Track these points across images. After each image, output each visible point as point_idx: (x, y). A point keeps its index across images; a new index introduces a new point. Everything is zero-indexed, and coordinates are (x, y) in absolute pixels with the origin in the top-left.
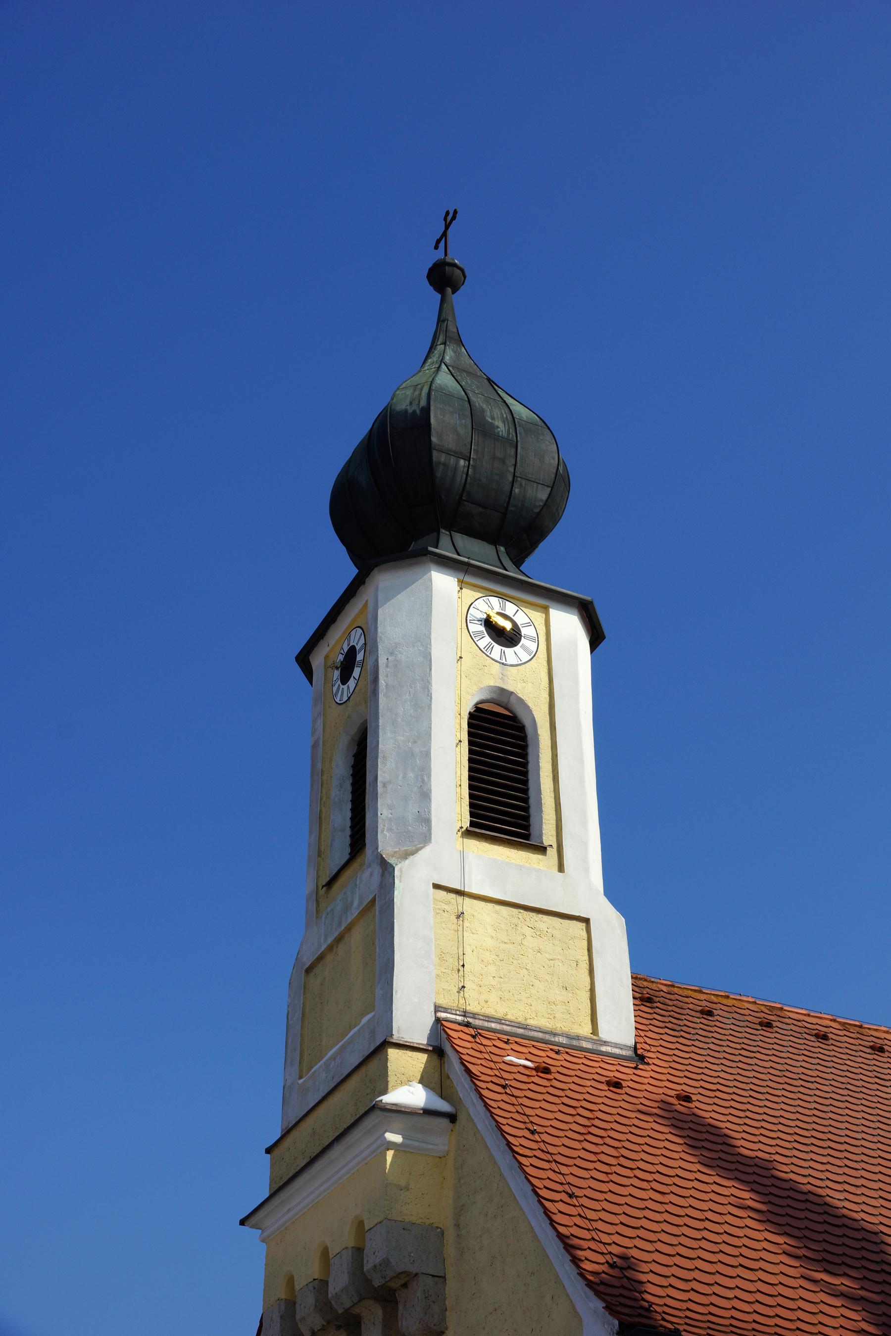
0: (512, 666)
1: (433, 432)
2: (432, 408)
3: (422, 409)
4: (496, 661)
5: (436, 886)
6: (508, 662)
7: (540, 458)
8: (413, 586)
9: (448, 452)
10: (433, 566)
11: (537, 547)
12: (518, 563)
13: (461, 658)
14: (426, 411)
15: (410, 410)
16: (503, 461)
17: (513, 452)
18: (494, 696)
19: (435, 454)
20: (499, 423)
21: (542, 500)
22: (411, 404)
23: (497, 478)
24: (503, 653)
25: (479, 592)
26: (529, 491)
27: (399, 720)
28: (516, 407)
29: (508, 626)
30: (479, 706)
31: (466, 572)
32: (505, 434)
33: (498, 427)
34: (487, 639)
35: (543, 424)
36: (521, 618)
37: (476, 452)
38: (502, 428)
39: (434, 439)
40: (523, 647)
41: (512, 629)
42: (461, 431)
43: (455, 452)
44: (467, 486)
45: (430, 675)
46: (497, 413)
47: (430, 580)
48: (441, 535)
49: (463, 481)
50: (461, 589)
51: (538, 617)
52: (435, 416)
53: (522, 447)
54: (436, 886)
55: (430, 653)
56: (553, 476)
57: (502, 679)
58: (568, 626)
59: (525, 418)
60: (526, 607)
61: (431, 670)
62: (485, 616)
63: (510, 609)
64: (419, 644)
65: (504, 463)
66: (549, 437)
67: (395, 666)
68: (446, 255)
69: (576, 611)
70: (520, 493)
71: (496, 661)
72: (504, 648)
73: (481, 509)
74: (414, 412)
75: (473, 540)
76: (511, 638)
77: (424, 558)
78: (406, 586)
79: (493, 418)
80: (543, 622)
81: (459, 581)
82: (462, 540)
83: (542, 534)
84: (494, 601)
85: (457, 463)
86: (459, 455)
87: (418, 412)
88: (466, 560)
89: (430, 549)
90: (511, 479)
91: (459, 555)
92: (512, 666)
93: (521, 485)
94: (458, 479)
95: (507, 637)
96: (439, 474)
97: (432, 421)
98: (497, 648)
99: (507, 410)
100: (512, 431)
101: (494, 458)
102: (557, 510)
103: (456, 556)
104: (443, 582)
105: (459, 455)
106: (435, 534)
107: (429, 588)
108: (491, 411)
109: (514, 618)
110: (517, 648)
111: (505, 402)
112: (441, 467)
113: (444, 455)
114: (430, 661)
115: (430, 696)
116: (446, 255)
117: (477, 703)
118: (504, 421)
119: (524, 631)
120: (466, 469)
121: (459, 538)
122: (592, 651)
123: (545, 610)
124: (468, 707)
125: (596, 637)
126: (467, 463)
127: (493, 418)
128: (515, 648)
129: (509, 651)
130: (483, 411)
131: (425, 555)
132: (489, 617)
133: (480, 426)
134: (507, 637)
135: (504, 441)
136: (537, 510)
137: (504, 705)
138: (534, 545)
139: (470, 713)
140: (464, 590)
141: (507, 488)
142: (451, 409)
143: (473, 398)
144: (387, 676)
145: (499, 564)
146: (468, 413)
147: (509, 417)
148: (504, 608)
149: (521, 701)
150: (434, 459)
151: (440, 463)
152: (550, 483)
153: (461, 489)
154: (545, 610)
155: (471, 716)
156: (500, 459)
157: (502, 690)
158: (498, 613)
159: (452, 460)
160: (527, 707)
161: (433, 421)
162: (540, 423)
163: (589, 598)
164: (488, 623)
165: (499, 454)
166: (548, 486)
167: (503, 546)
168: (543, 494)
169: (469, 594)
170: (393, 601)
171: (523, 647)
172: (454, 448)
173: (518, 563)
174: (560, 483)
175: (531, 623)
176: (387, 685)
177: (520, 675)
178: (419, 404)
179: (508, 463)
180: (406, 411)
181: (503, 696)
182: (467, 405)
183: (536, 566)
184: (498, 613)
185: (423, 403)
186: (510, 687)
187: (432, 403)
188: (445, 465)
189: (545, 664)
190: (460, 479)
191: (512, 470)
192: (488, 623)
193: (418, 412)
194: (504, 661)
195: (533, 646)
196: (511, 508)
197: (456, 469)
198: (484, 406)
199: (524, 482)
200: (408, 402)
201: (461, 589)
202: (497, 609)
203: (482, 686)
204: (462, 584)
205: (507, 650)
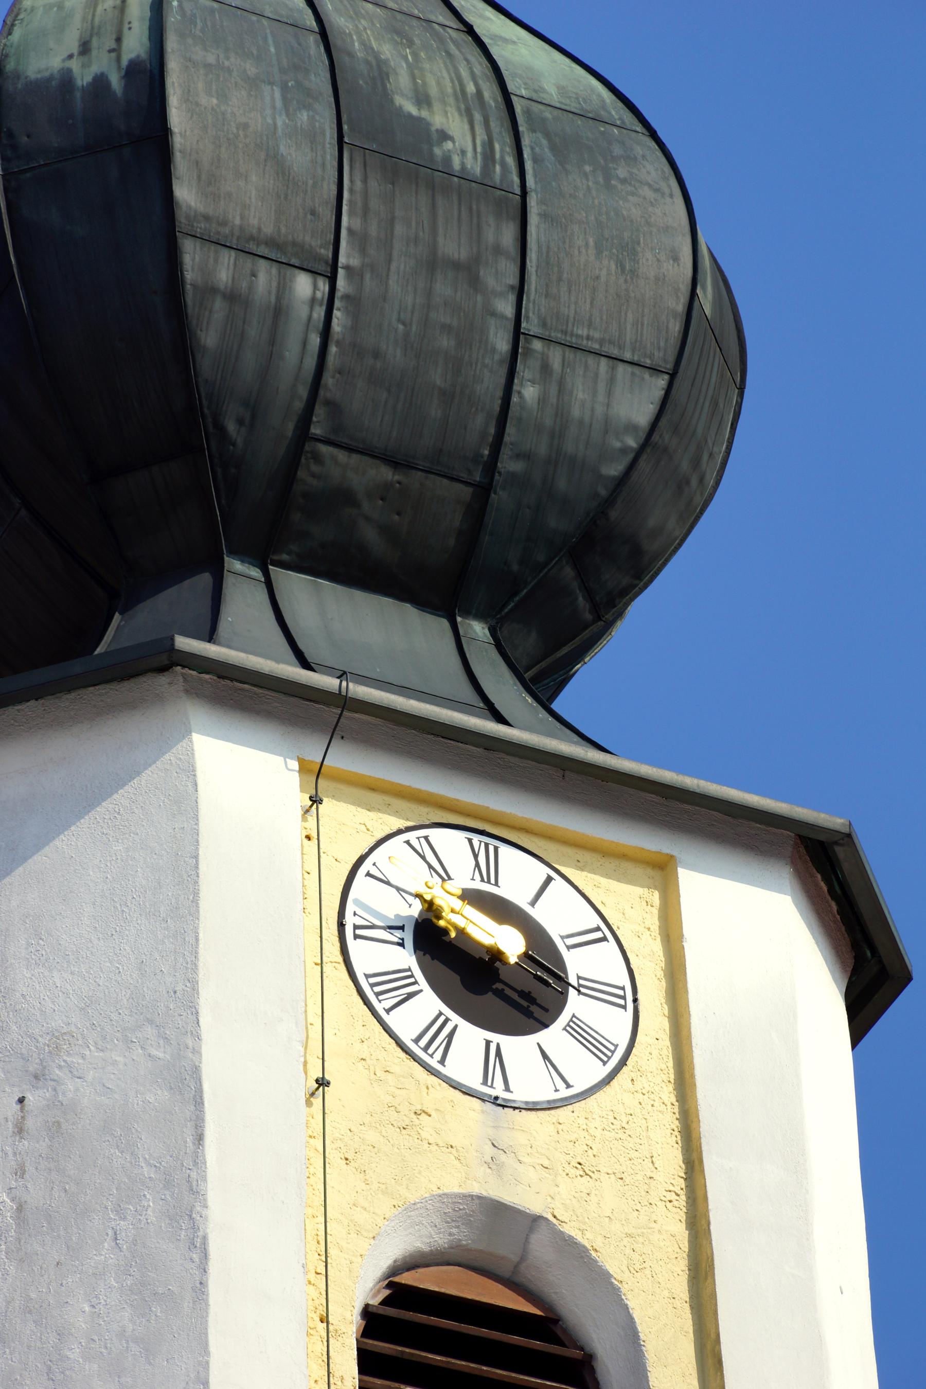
0: (533, 1107)
1: (181, 165)
2: (173, 65)
3: (132, 71)
4: (468, 1092)
5: (430, 1116)
6: (519, 1095)
7: (615, 254)
8: (121, 797)
9: (245, 247)
10: (197, 714)
11: (620, 615)
12: (544, 681)
13: (322, 1083)
14: (149, 78)
15: (83, 77)
16: (469, 272)
17: (508, 236)
18: (463, 1235)
19: (192, 257)
20: (447, 119)
21: (631, 428)
22: (85, 48)
23: (445, 342)
24: (493, 1059)
25: (387, 809)
26: (580, 393)
27: (74, 1353)
28: (518, 50)
29: (511, 944)
30: (406, 1278)
31: (334, 732)
32: (475, 167)
33: (444, 136)
34: (428, 1004)
35: (628, 118)
36: (560, 914)
37: (361, 241)
38: (461, 140)
39: (185, 193)
40: (576, 1030)
41: (526, 956)
42: (297, 157)
43: (271, 243)
44: (328, 379)
45: (198, 1161)
46: (437, 76)
47: (190, 771)
48: (229, 581)
49: (310, 363)
50: (316, 800)
51: (631, 904)
52: (188, 98)
53: (544, 216)
54: (430, 1116)
55: (196, 1072)
56: (676, 327)
57: (492, 1163)
58: (755, 939)
59: (552, 93)
60: (581, 866)
61: (200, 1139)
62: (416, 909)
63: (518, 876)
64: (150, 1031)
65: (475, 282)
66: (653, 167)
67: (55, 1129)
68: (533, 903)
69: (784, 874)
70: (542, 400)
71: (468, 1092)
72: (495, 1038)
73: (387, 474)
74: (100, 81)
75: (359, 595)
76: (527, 995)
77: (163, 680)
78: (88, 801)
79: (423, 99)
80: (654, 922)
81: (304, 768)
82: (314, 602)
83: (641, 567)
84: (453, 845)
85: (283, 288)
86: (287, 257)
87: (116, 81)
88: (330, 683)
89: (184, 643)
90: (503, 344)
91: (306, 664)
92: (533, 1107)
93: (546, 369)
94: (291, 352)
95: (500, 987)
96: (209, 337)
97: (176, 117)
98: (470, 1038)
99: (480, 66)
100: (503, 149)
101: (432, 264)
102: (696, 463)
103: (293, 671)
104: (239, 781)
105: (287, 257)
106: (205, 579)
107: (184, 803)
108: (414, 70)
109: (538, 914)
110: (553, 1037)
111: (469, 30)
112: (219, 304)
113: (227, 258)
114: (198, 1101)
115: (199, 1248)
116: (533, 903)
117: (396, 1269)
118: (469, 107)
119: (577, 964)
120: (319, 313)
121: (302, 593)
122: (857, 1036)
123: (662, 872)
124: (358, 1286)
125: (870, 983)
126: (323, 286)
127: (423, 99)
128: (543, 1037)
129: (518, 1049)
130: (380, 72)
131: (163, 669)
132: (431, 907)
133: (366, 130)
134: (500, 987)
135: (471, 190)
136: (614, 469)
137: (506, 1273)
138: (607, 608)
139: (367, 1313)
140: (328, 806)
141: (489, 383)
142: (251, 69)
143: (338, 21)
144: (20, 1172)
145: (467, 693)
146: (320, 80)
147: (490, 93)
148: (492, 873)
149: (576, 1254)
150: (190, 275)
151: (214, 290)
152: (665, 356)
153: (303, 392)
154: (662, 872)
155: (373, 1323)
156: (456, 266)
157: (496, 1212)
158: (469, 896)
159: (265, 278)
160: (601, 1281)
161: (177, 117)
162: (617, 111)
163: (833, 820)
164: (430, 937)
165: (452, 246)
166: (655, 370)
167: (481, 616)
168: (635, 404)
169: (350, 823)
170: (38, 861)
171: (576, 1030)
172: (268, 230)
173: (544, 681)
174: (706, 353)
175: (606, 931)
176: (20, 1209)
177: (559, 1150)
178: (116, 52)
179: (490, 281)
180: (66, 81)
181: (498, 1232)
182: (313, 45)
183: (632, 687)
184: (469, 896)
185: (135, 44)
186: (527, 1197)
187: (172, 43)
188: (232, 297)
189: (668, 1094)
190: (297, 351)
191: (507, 308)
192: (430, 937)
193: (116, 81)
194: (498, 1090)
195: (613, 1024)
196: (508, 465)
197: (279, 311)
198: (387, 50)
199: (556, 357)
200: (72, 42)
201: (316, 800)
202: (464, 876)
203: (412, 1198)
204: (318, 782)
205: (510, 1044)
